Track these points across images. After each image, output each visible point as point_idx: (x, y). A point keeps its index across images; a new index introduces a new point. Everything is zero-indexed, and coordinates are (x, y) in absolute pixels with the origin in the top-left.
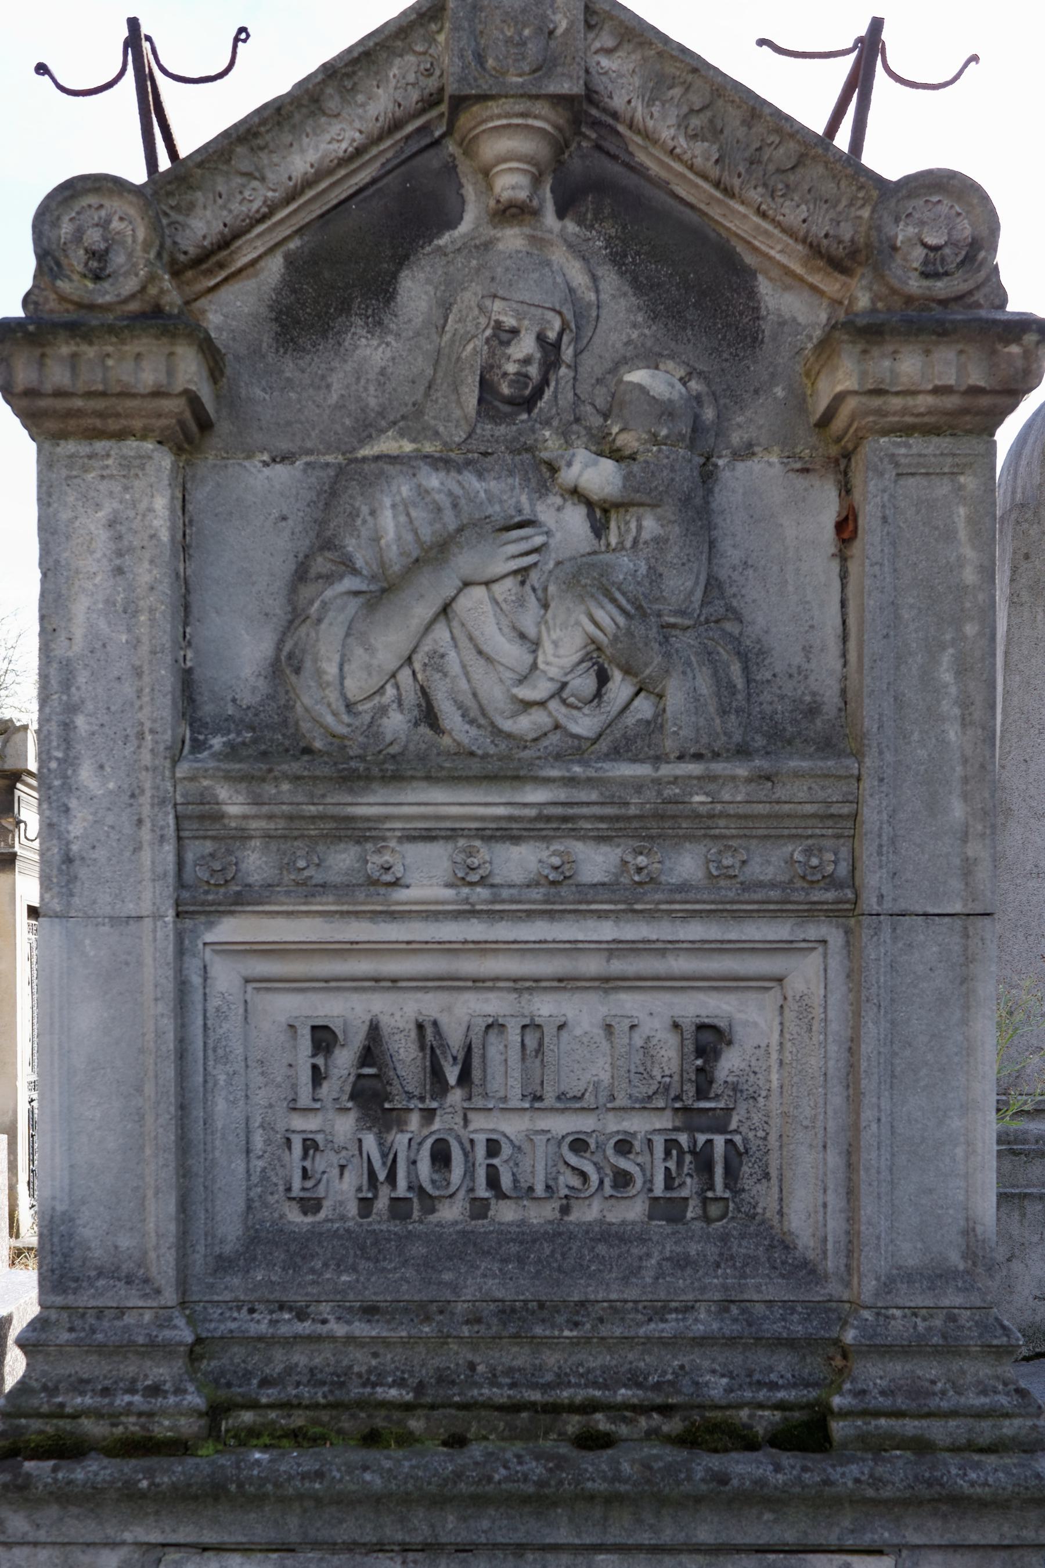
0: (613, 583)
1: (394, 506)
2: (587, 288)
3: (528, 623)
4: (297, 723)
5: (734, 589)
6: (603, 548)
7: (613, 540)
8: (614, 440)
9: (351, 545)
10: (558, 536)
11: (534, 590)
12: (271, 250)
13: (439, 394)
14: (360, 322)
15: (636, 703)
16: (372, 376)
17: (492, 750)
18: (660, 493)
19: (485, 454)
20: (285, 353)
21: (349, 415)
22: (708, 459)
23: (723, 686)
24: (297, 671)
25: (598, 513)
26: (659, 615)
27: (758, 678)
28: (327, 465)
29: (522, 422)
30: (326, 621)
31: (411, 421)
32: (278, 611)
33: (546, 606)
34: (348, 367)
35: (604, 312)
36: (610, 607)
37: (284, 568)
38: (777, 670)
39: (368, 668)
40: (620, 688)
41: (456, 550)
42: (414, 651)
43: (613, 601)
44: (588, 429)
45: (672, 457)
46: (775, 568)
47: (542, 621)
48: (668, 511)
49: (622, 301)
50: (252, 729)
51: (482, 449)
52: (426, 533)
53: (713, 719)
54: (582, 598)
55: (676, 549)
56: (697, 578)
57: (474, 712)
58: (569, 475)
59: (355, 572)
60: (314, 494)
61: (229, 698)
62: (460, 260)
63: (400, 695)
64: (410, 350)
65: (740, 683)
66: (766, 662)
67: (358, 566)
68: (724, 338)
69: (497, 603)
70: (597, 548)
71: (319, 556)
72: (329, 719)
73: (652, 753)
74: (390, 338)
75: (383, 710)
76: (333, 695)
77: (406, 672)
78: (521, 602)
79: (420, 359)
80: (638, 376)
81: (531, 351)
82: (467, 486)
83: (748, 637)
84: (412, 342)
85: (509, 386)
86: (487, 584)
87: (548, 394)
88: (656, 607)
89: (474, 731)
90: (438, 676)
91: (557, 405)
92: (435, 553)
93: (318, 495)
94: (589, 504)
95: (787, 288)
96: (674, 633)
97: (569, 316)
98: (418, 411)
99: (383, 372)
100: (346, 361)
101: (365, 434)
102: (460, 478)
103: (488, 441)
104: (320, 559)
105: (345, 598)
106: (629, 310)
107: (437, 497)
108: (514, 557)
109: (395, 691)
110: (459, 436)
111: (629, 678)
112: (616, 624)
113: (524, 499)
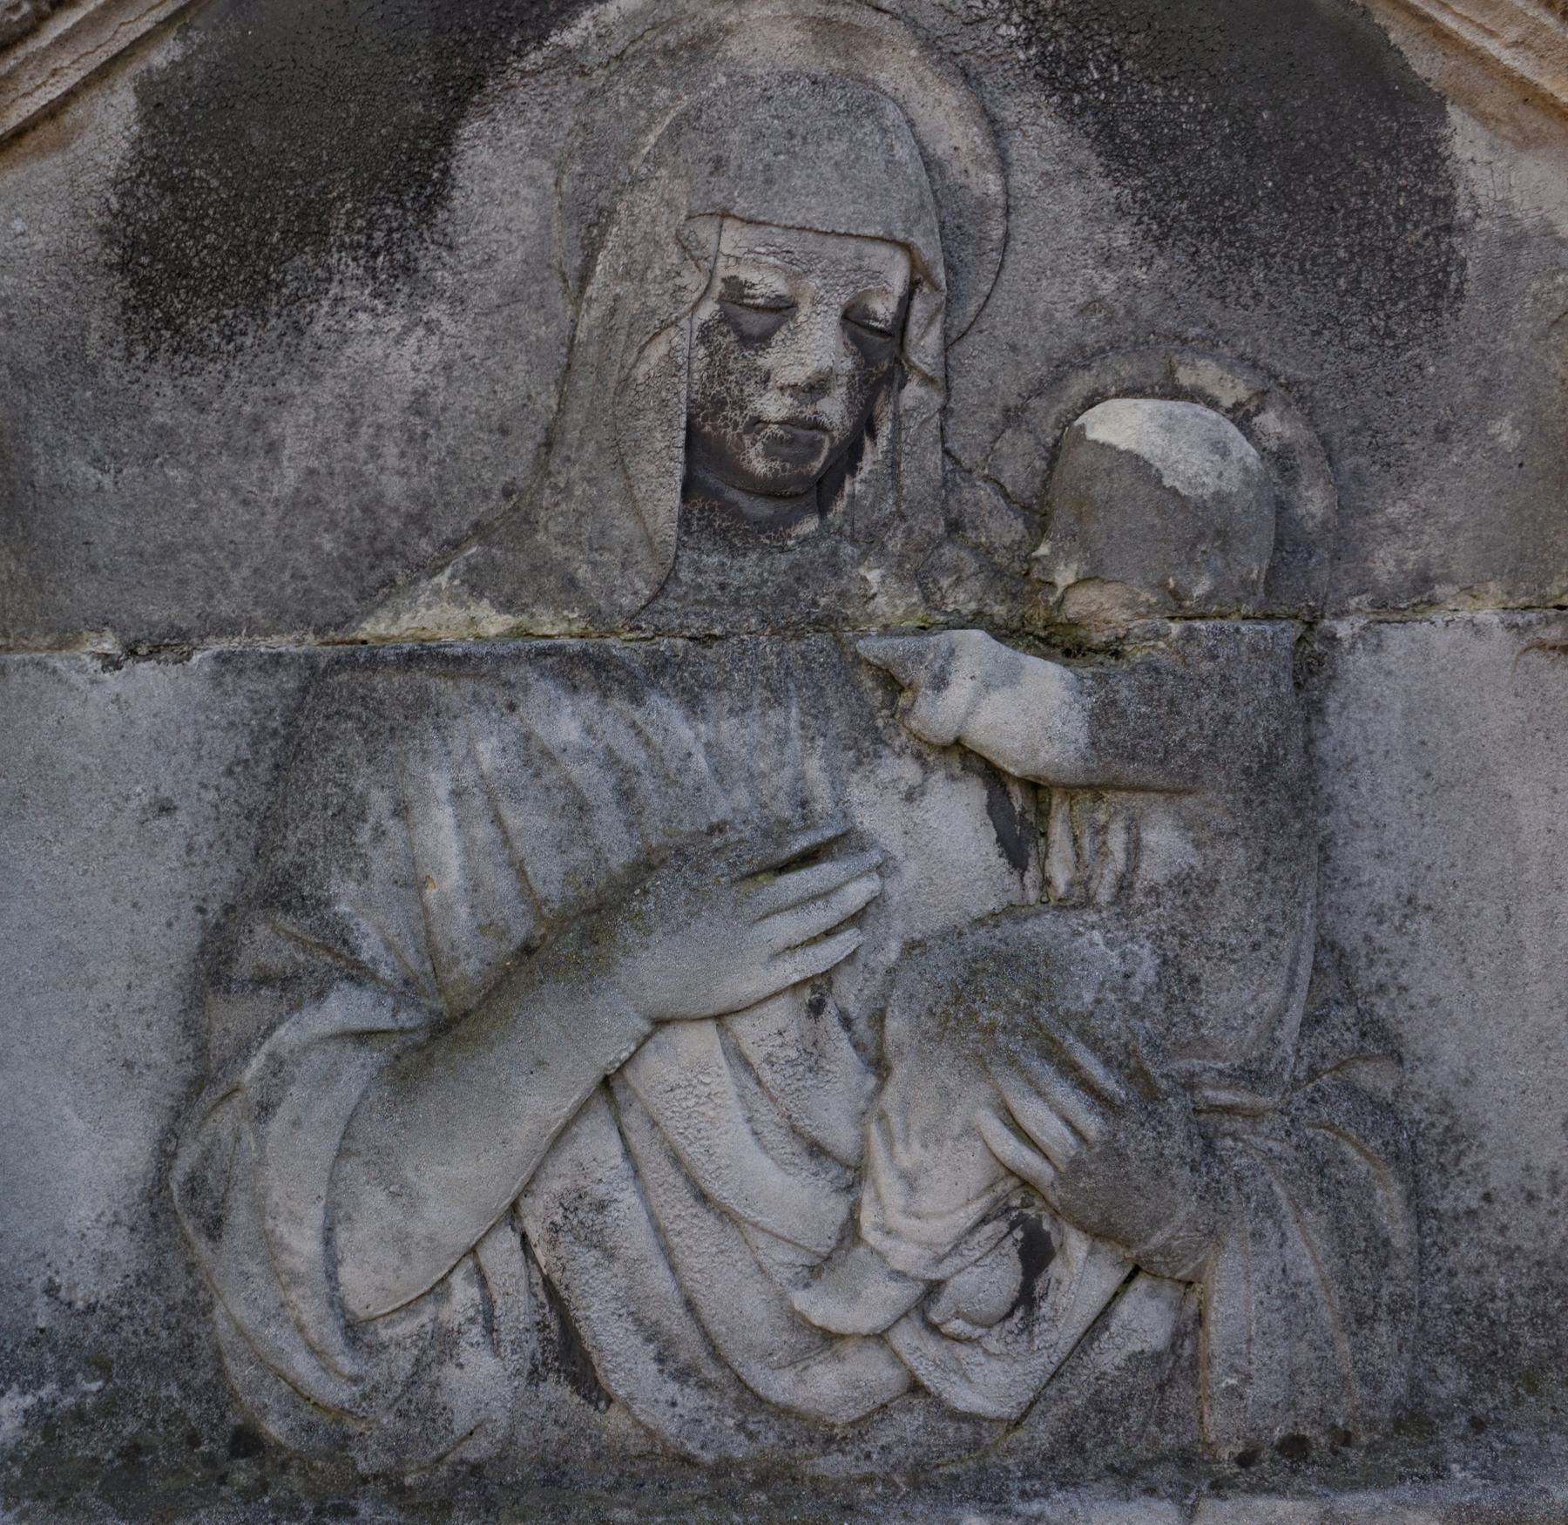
0: (1065, 1021)
1: (457, 795)
2: (977, 159)
3: (833, 1113)
4: (218, 1355)
5: (1381, 971)
6: (1032, 895)
7: (1061, 875)
8: (1061, 601)
9: (345, 896)
10: (911, 870)
11: (846, 1022)
12: (102, 74)
13: (575, 472)
14: (355, 270)
15: (1125, 1309)
16: (390, 415)
17: (740, 1449)
18: (1194, 758)
19: (706, 640)
20: (150, 359)
21: (333, 525)
22: (1310, 625)
23: (1361, 1248)
24: (215, 1228)
25: (1018, 800)
26: (1190, 1084)
27: (1444, 1206)
28: (277, 659)
29: (804, 541)
30: (283, 1114)
31: (497, 540)
32: (157, 1056)
33: (879, 1066)
34: (324, 393)
35: (1022, 223)
36: (1062, 1092)
37: (173, 942)
38: (1493, 1183)
39: (401, 1241)
40: (1081, 1276)
41: (633, 938)
42: (526, 1191)
43: (1069, 1069)
44: (983, 552)
45: (1225, 651)
46: (1491, 911)
47: (868, 1112)
48: (1215, 803)
49: (1072, 191)
50: (101, 1367)
51: (697, 625)
52: (549, 875)
53: (1330, 1342)
54: (981, 1064)
55: (1235, 907)
56: (1293, 973)
57: (690, 1349)
58: (941, 712)
59: (359, 974)
60: (244, 742)
61: (39, 1283)
62: (623, 91)
63: (488, 1300)
64: (492, 342)
65: (1400, 1234)
66: (1466, 1163)
67: (365, 956)
68: (1355, 287)
69: (747, 1065)
70: (1014, 897)
71: (262, 928)
72: (302, 1366)
73: (1169, 1439)
74: (436, 311)
75: (444, 1342)
76: (310, 1309)
77: (507, 1240)
78: (813, 1059)
79: (519, 367)
80: (1121, 425)
81: (827, 362)
82: (657, 739)
83: (1417, 1096)
84: (498, 320)
85: (768, 454)
86: (719, 1018)
87: (872, 457)
88: (1182, 1064)
89: (690, 1400)
90: (592, 1256)
91: (898, 488)
92: (572, 938)
93: (255, 744)
94: (992, 775)
95: (1528, 142)
96: (1227, 1126)
97: (930, 250)
98: (517, 514)
99: (419, 404)
100: (317, 377)
101: (379, 573)
102: (637, 716)
103: (712, 601)
104: (262, 931)
105: (333, 1048)
106: (1091, 218)
107: (576, 772)
108: (791, 949)
109: (475, 1292)
110: (633, 590)
111: (1104, 1247)
112: (1076, 1131)
113: (814, 768)
